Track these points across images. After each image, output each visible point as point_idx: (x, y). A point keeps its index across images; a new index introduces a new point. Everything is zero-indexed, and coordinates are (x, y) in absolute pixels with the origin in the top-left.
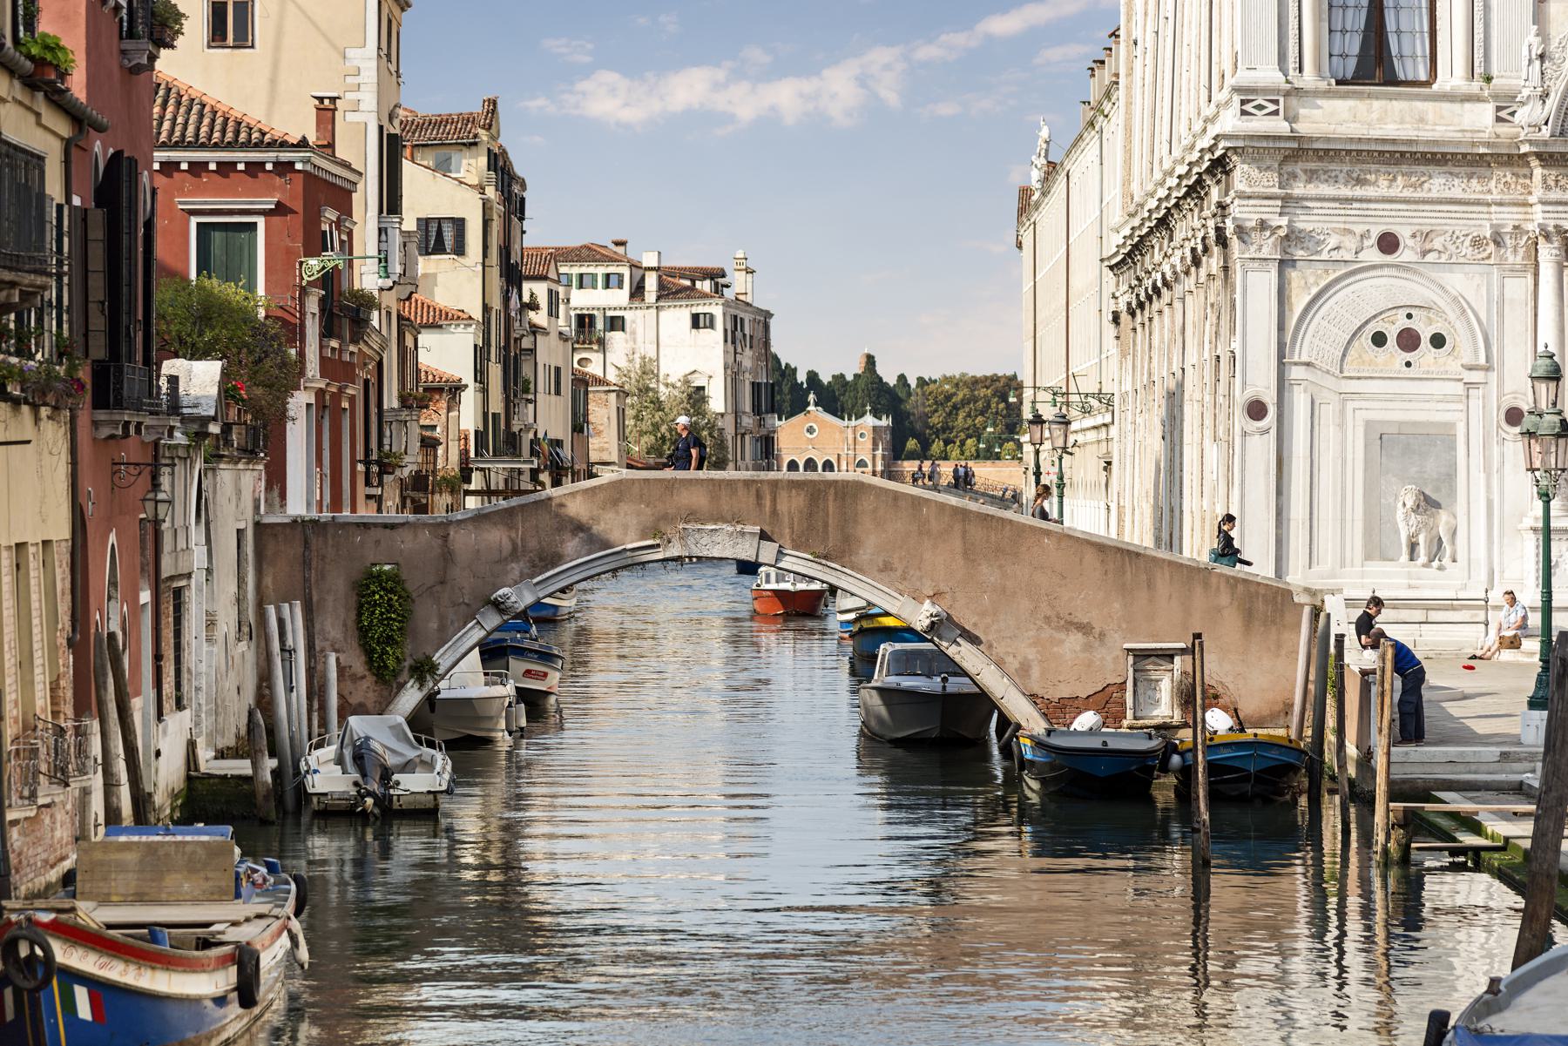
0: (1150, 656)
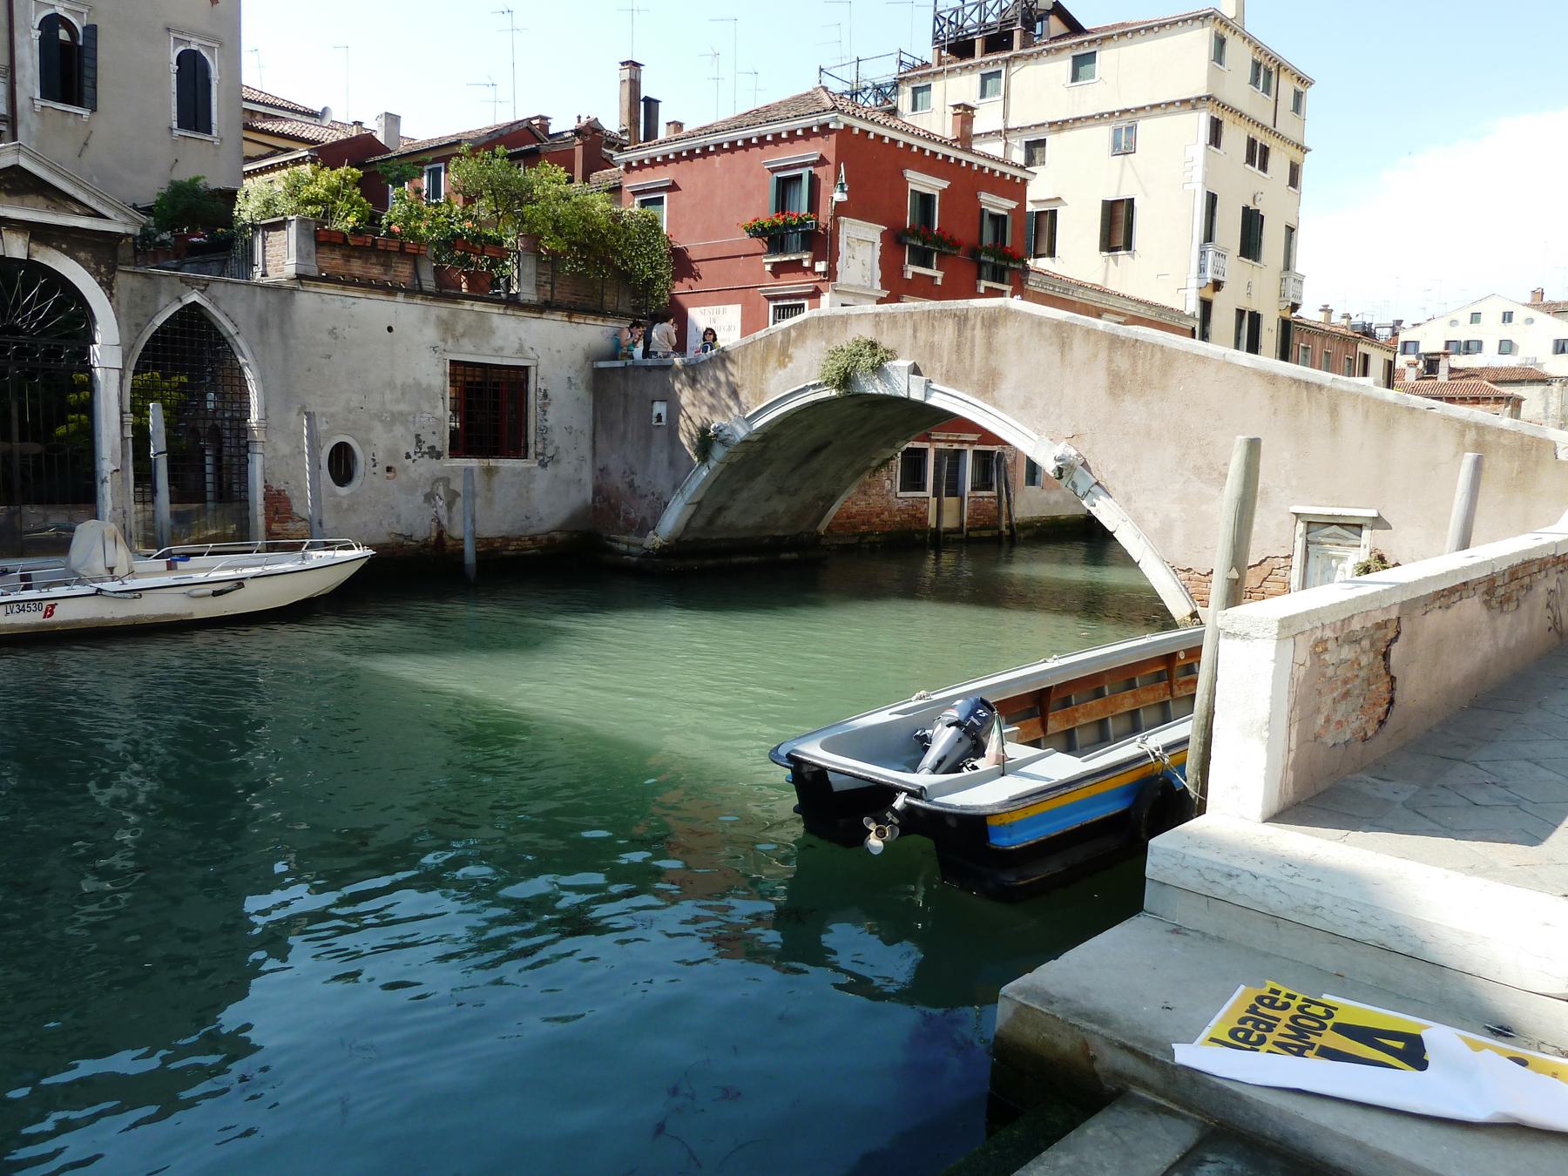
0: (1333, 524)
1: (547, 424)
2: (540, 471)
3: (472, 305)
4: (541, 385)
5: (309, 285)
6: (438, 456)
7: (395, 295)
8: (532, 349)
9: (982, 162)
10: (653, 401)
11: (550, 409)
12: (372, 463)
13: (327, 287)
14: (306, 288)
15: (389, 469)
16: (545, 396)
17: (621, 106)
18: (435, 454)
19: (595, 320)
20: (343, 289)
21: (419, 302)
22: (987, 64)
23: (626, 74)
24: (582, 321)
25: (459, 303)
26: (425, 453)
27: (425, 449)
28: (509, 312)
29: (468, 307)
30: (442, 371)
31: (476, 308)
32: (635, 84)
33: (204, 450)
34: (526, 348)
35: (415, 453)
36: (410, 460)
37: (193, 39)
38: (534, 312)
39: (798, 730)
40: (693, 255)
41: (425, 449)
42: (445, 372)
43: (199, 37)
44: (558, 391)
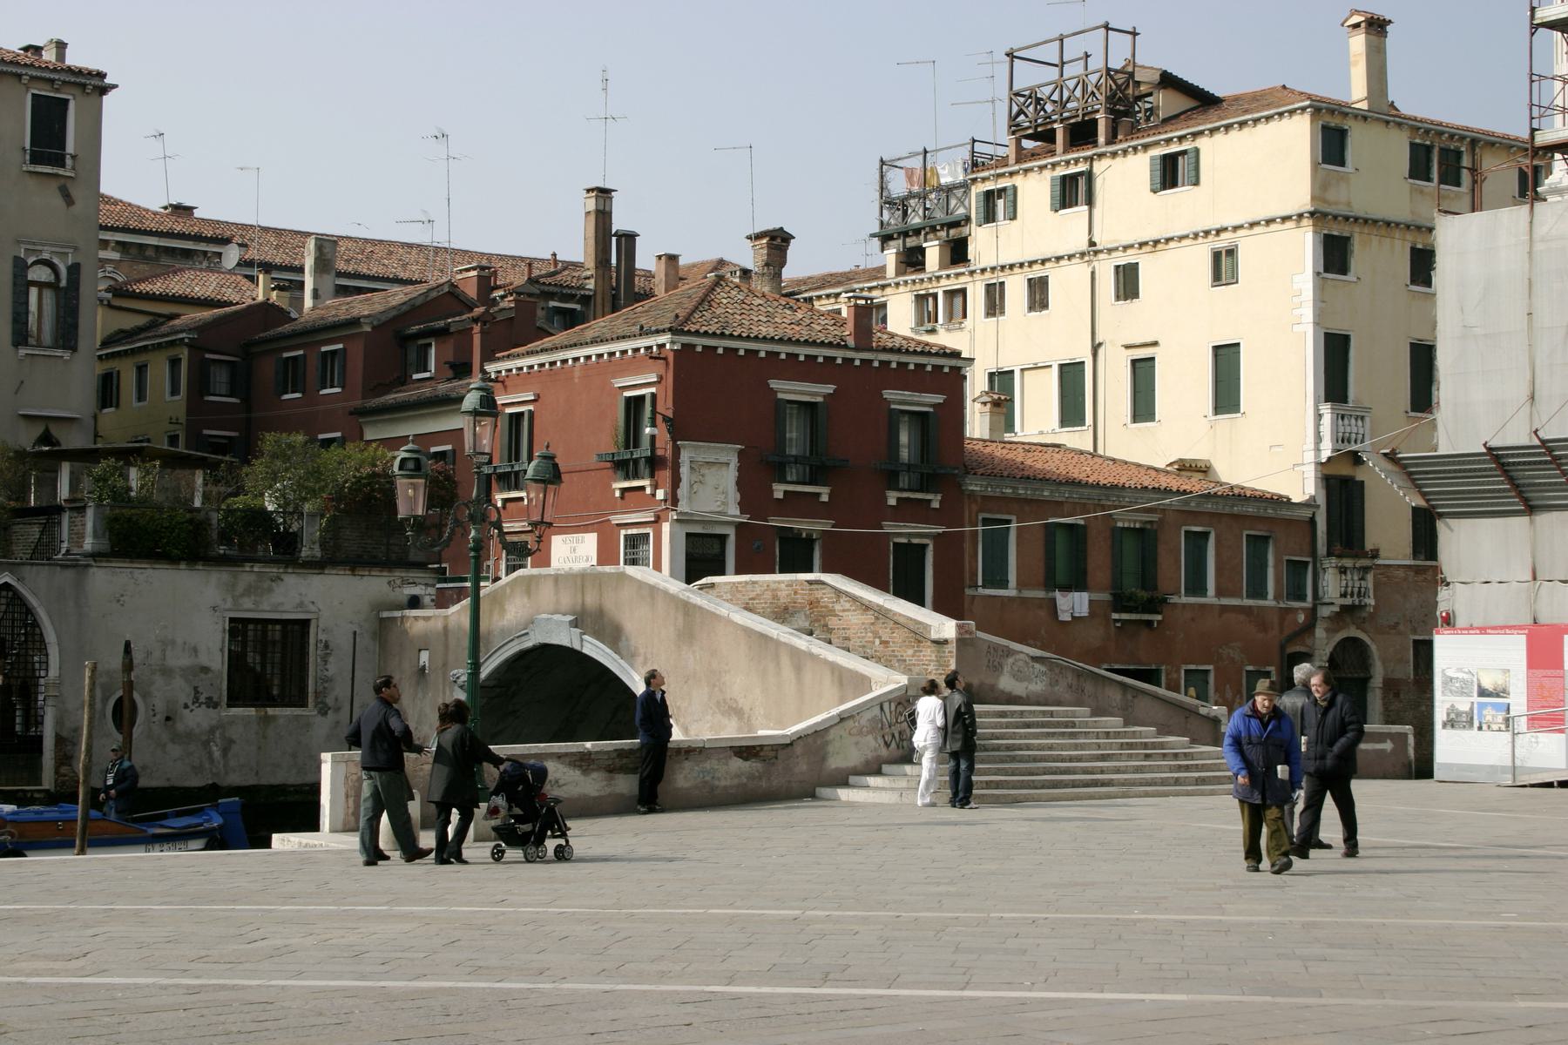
1: (329, 674)
2: (320, 719)
3: (252, 567)
4: (322, 637)
5: (101, 561)
6: (216, 705)
7: (179, 564)
8: (313, 603)
9: (885, 357)
10: (420, 650)
11: (331, 659)
12: (152, 713)
13: (117, 562)
14: (99, 564)
15: (168, 719)
16: (327, 646)
17: (586, 245)
18: (212, 704)
19: (381, 571)
20: (131, 562)
21: (201, 568)
22: (1068, 163)
23: (591, 205)
24: (367, 573)
25: (239, 566)
26: (202, 703)
27: (202, 699)
28: (290, 570)
29: (248, 569)
30: (221, 628)
31: (256, 569)
32: (603, 217)
33: (15, 705)
34: (306, 603)
35: (194, 703)
36: (188, 711)
37: (45, 248)
38: (315, 568)
39: (162, 826)
40: (562, 470)
41: (202, 699)
42: (224, 630)
43: (51, 245)
44: (342, 641)
